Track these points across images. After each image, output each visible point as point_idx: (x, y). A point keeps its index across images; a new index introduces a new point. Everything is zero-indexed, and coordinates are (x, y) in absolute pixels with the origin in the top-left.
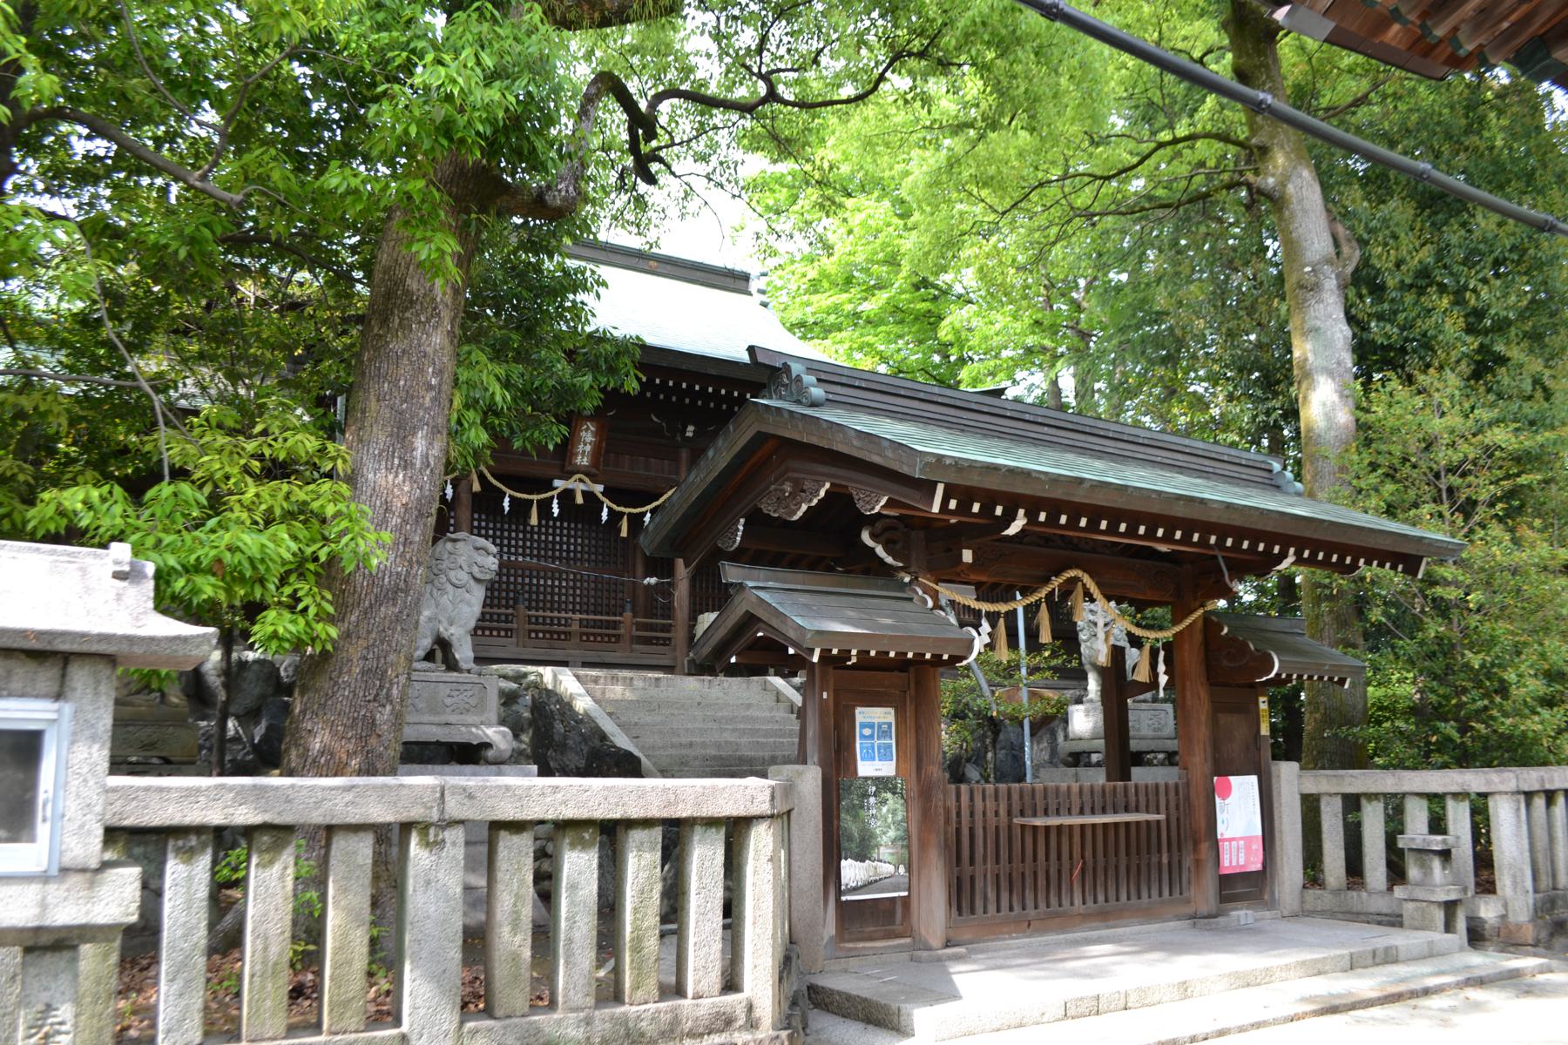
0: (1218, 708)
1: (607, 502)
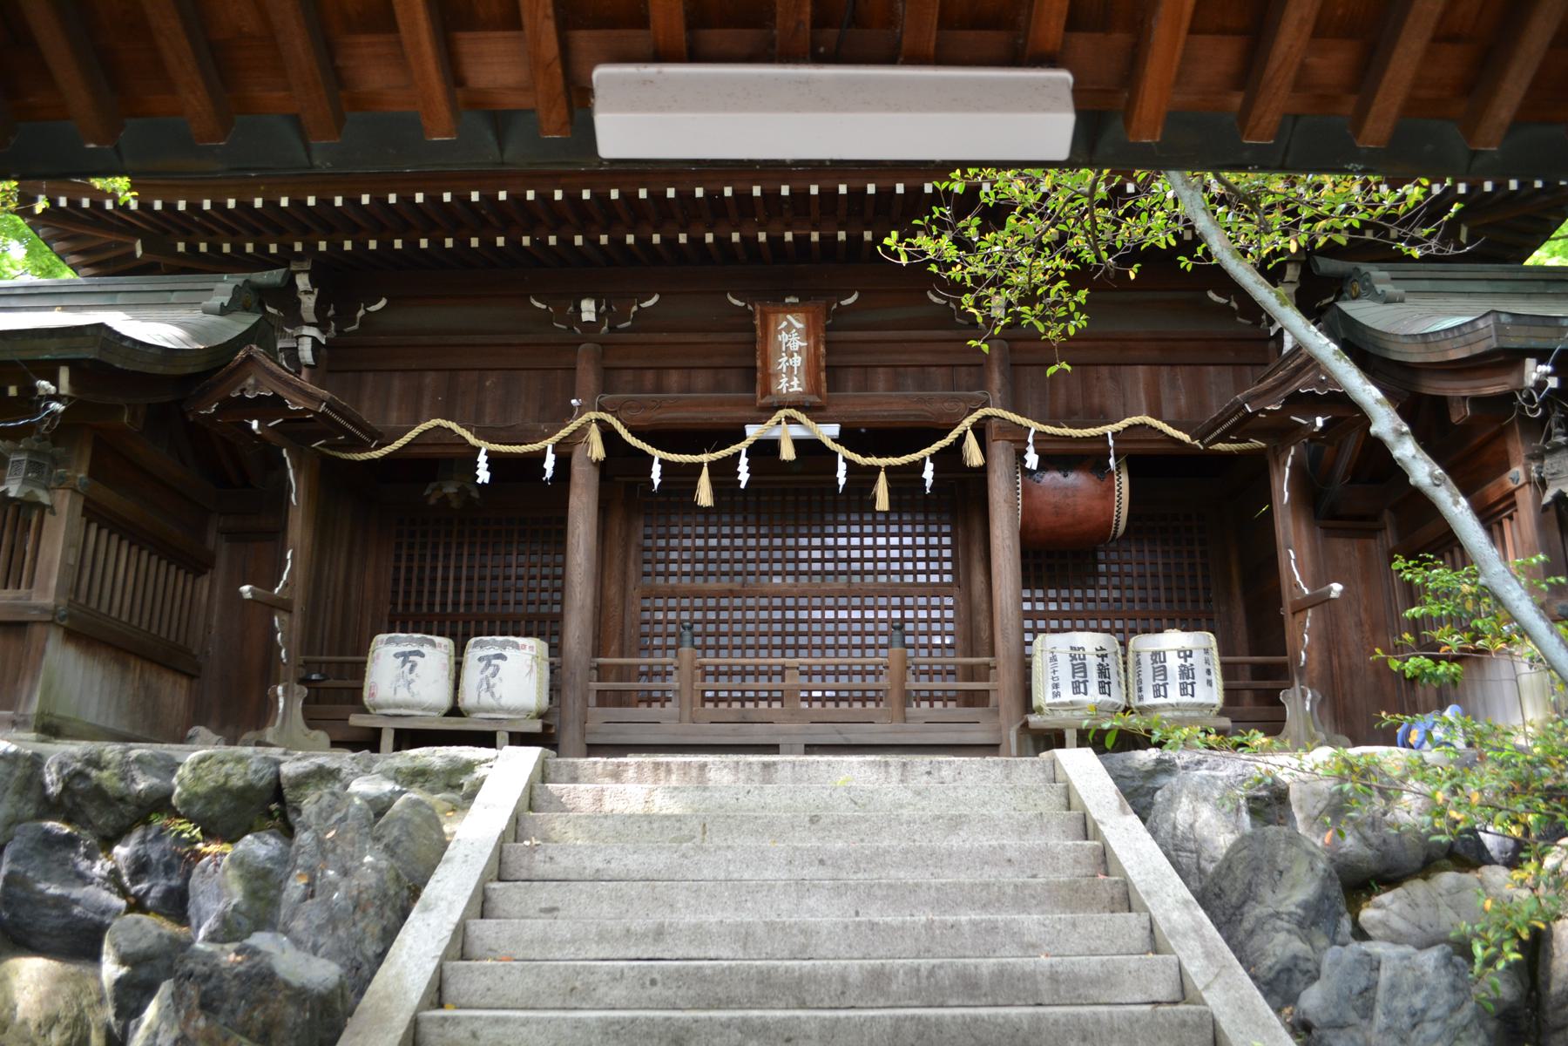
1: (842, 452)
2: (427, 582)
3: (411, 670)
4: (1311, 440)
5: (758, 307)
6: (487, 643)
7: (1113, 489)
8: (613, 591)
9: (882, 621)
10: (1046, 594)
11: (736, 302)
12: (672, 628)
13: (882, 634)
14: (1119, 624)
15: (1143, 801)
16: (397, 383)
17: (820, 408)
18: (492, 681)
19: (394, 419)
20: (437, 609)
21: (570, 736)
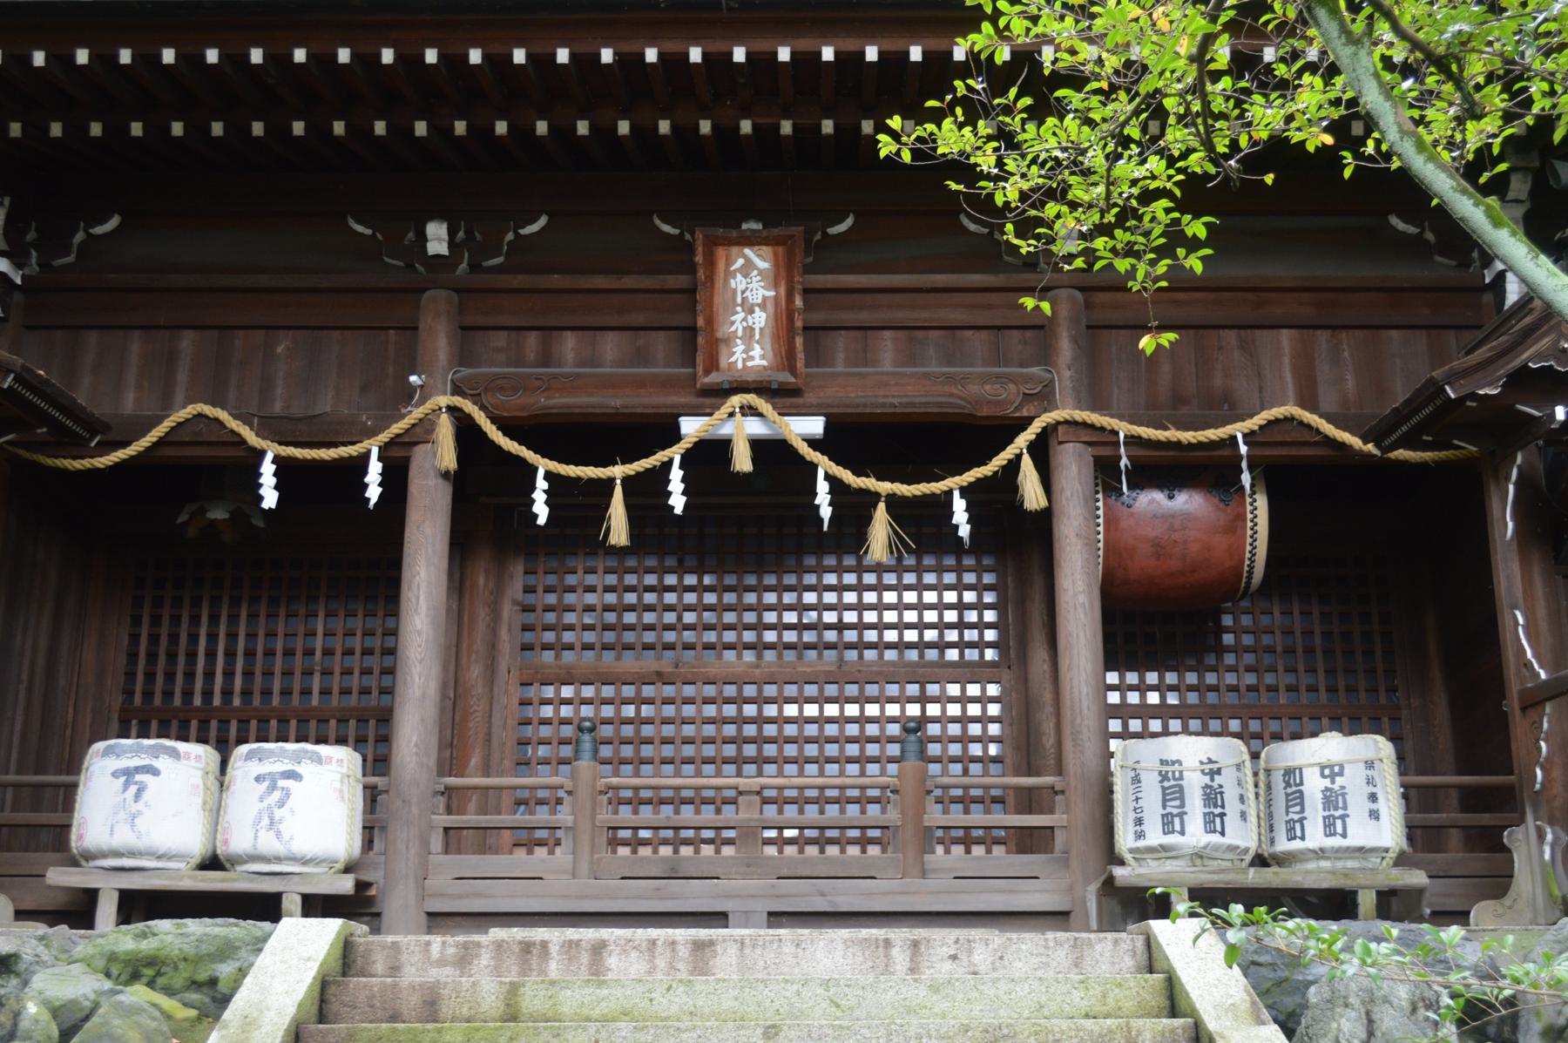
0: (1301, 861)
1: (825, 465)
2: (182, 659)
3: (137, 796)
4: (1548, 443)
5: (699, 236)
6: (271, 753)
7: (1243, 518)
8: (475, 673)
9: (893, 720)
10: (1142, 679)
11: (666, 228)
12: (567, 731)
13: (892, 740)
14: (1254, 725)
15: (1290, 1002)
16: (135, 346)
17: (795, 392)
18: (278, 813)
19: (129, 403)
20: (197, 701)
21: (399, 902)
